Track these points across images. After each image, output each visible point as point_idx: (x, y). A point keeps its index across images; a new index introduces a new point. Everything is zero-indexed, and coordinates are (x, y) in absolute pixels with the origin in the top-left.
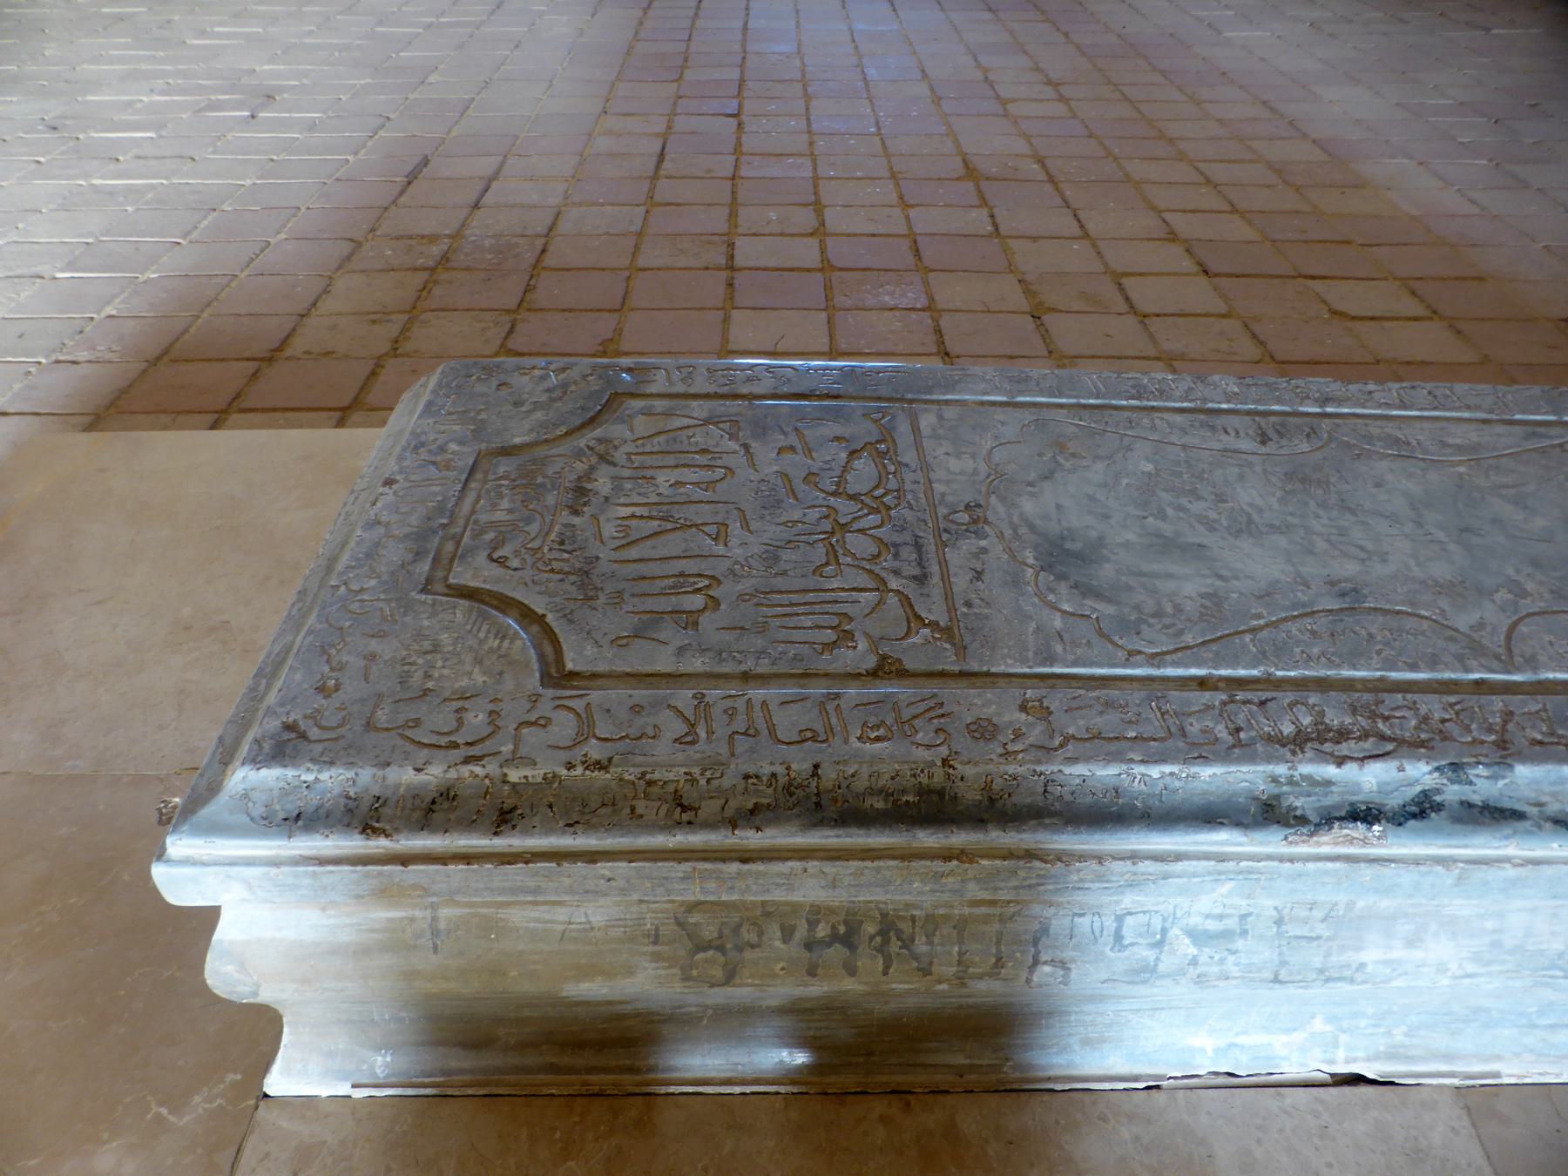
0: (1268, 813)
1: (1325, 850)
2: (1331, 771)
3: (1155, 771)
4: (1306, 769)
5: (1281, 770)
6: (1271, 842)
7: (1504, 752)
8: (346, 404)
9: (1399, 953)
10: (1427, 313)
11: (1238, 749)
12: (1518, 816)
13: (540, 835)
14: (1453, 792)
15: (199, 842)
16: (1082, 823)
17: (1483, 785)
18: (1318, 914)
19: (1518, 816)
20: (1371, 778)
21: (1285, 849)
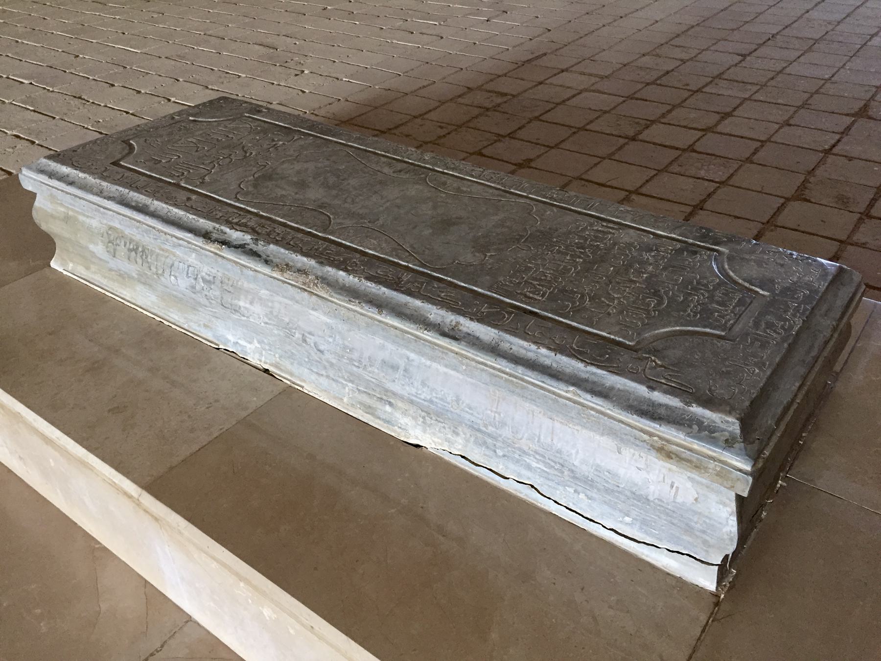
0: (206, 236)
1: (212, 249)
2: (227, 230)
3: (191, 216)
4: (223, 228)
5: (217, 226)
6: (199, 242)
7: (271, 239)
8: (383, 129)
9: (248, 306)
10: (543, 118)
11: (208, 216)
12: (259, 256)
13: (610, 406)
14: (252, 246)
15: (648, 422)
16: (536, 370)
17: (260, 247)
18: (230, 283)
19: (259, 256)
20: (235, 235)
21: (358, 309)
